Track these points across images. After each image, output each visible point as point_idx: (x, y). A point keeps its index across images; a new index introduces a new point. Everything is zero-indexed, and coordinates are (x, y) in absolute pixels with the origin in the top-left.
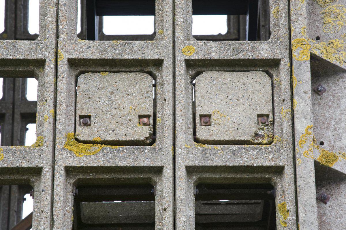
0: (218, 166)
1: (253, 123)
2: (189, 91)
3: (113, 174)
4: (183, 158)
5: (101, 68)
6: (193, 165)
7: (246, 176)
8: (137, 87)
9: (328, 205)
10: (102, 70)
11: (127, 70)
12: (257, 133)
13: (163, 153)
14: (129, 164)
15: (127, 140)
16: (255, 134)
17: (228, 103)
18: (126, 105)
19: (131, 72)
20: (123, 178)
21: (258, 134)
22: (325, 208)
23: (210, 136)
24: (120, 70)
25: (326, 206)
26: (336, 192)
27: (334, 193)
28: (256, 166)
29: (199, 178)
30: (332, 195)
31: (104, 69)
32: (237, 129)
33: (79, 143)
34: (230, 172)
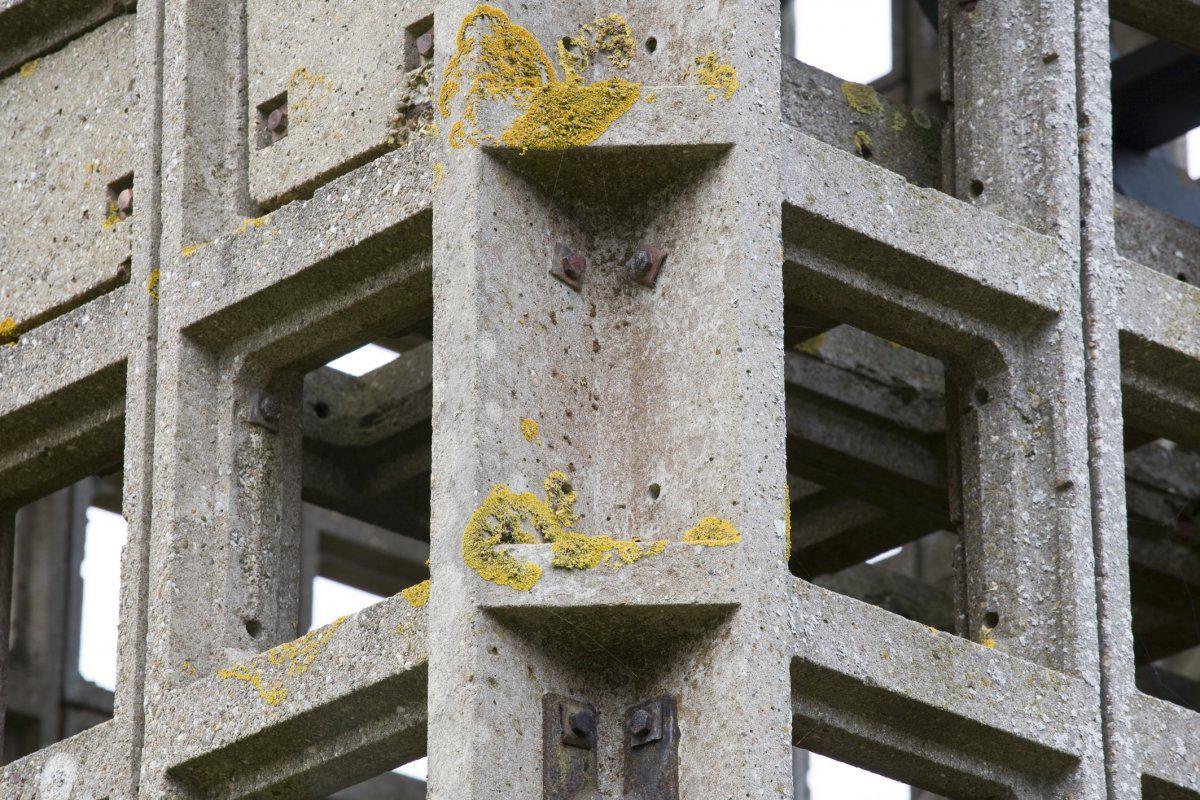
0: (265, 290)
1: (394, 67)
2: (234, 26)
3: (37, 441)
4: (176, 303)
5: (19, 52)
6: (200, 317)
7: (368, 292)
8: (107, 79)
9: (659, 291)
10: (25, 56)
11: (86, 23)
12: (409, 104)
13: (126, 306)
14: (42, 387)
15: (78, 292)
16: (402, 110)
17: (329, 24)
18: (734, 32)
19: (91, 29)
20: (71, 442)
21: (413, 106)
22: (653, 303)
23: (283, 177)
24: (66, 33)
25: (656, 296)
26: (684, 230)
27: (677, 232)
28: (361, 243)
29: (252, 356)
30: (672, 244)
31: (27, 51)
32: (353, 114)
33: (16, 340)
34: (301, 303)
